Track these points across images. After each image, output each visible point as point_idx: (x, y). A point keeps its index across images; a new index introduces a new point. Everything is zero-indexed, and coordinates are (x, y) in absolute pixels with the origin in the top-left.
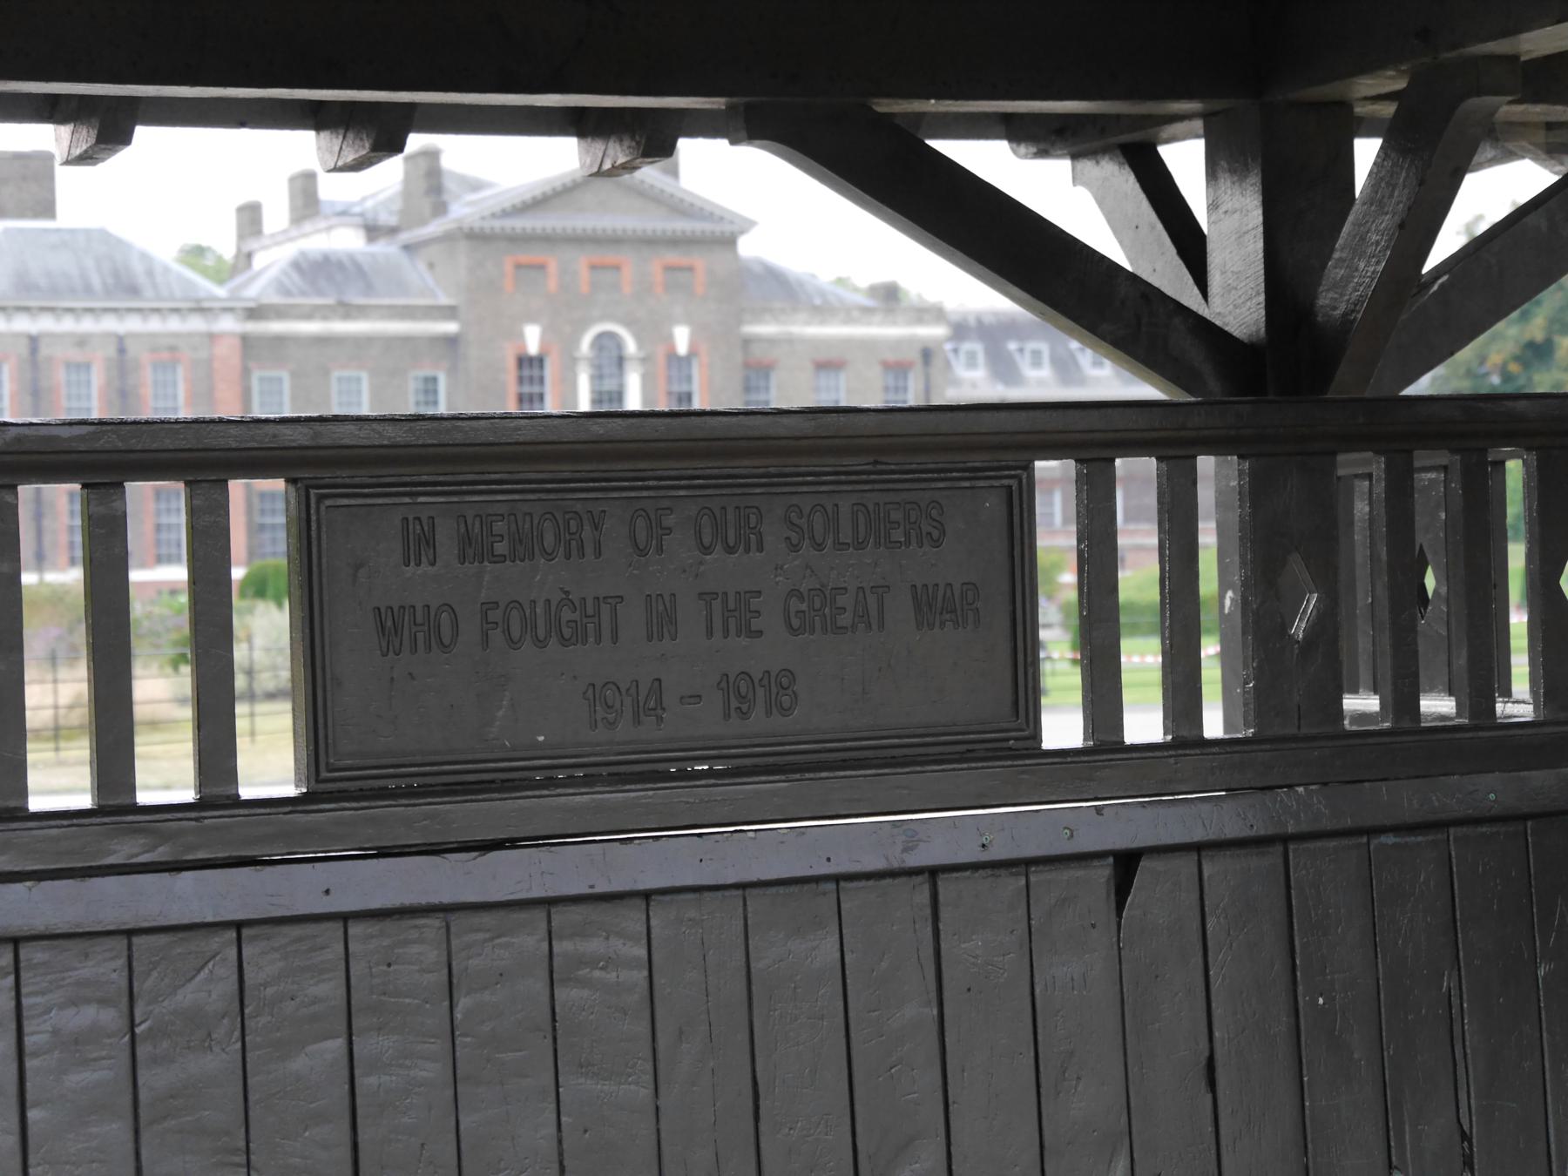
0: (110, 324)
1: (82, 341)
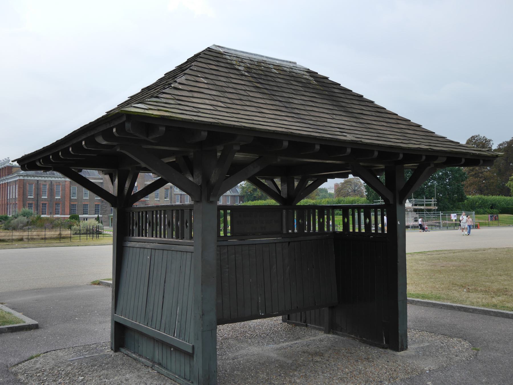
0: (50, 179)
1: (45, 181)
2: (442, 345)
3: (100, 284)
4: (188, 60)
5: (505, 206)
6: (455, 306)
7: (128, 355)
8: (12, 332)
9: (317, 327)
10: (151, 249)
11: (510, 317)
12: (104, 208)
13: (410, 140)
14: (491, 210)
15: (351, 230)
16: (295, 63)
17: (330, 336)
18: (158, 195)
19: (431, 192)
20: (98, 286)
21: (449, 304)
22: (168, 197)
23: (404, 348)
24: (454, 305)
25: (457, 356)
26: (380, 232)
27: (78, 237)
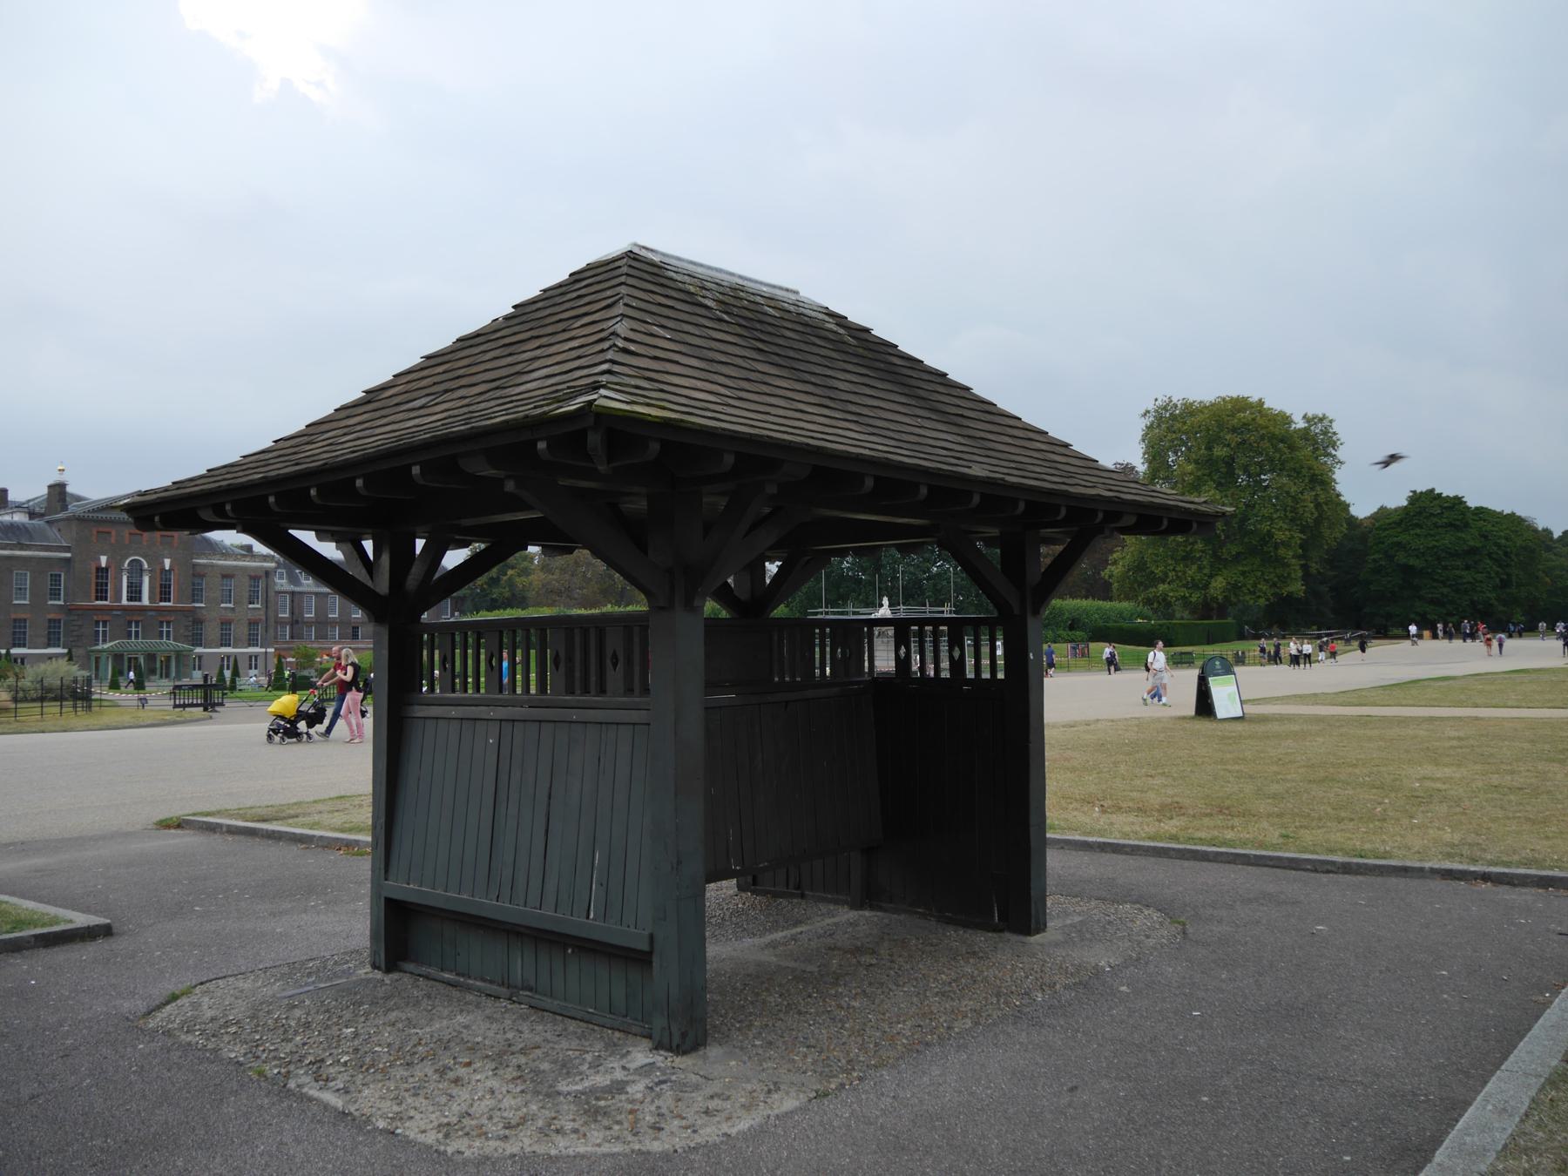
2: (1107, 918)
3: (184, 825)
4: (571, 275)
5: (1101, 624)
6: (1092, 842)
7: (427, 977)
8: (46, 946)
9: (829, 896)
10: (501, 720)
11: (1211, 858)
12: (76, 628)
13: (1071, 477)
14: (1070, 633)
15: (970, 675)
16: (796, 293)
17: (867, 913)
18: (230, 595)
19: (937, 590)
20: (179, 832)
21: (1077, 837)
22: (258, 598)
23: (1041, 927)
24: (1090, 839)
25: (1148, 937)
26: (986, 675)
27: (36, 709)
